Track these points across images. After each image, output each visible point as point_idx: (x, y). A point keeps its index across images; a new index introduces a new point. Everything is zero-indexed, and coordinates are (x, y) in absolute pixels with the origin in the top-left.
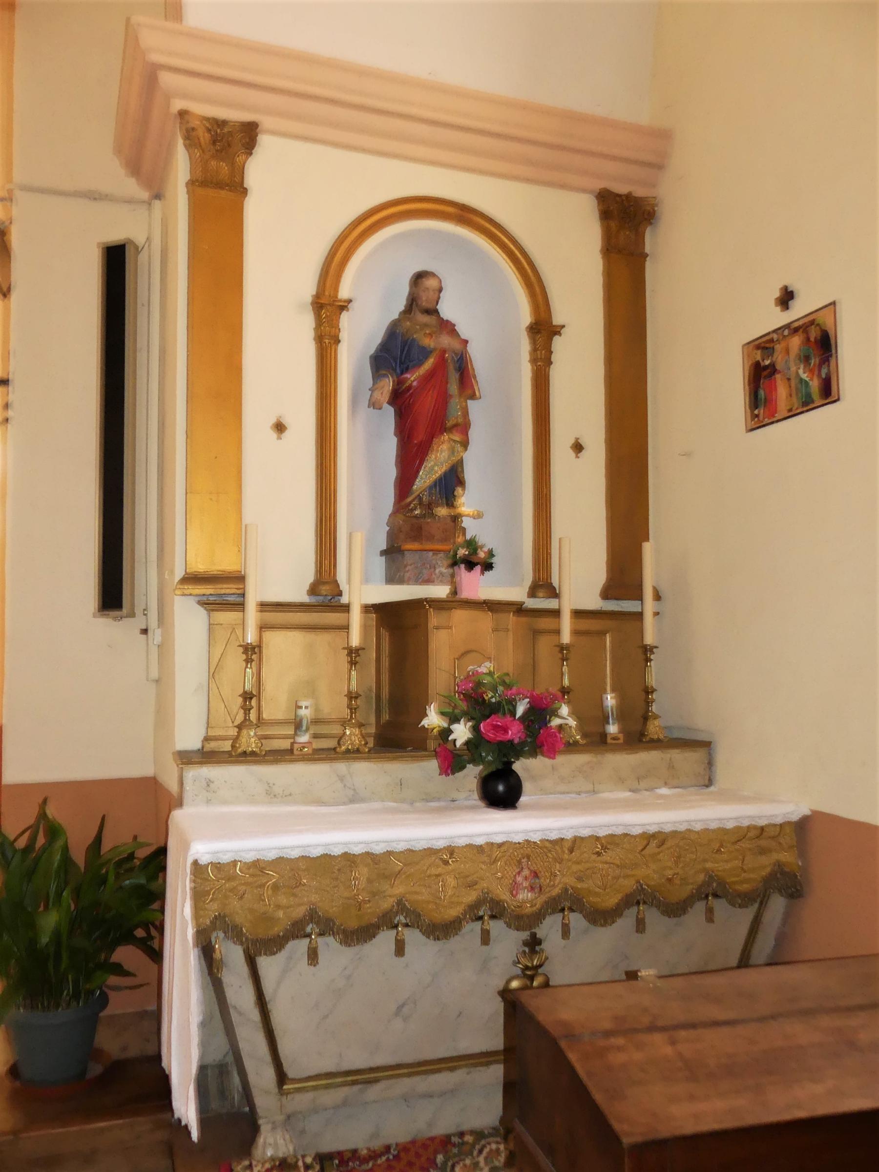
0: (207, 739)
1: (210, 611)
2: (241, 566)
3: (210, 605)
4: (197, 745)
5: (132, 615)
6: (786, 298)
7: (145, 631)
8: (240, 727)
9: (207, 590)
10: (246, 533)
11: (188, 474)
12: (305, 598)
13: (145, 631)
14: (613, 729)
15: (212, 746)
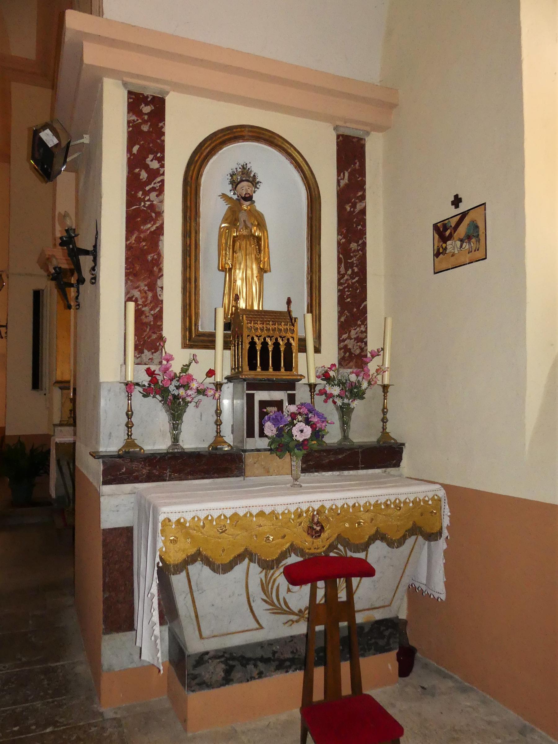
0: (61, 421)
1: (62, 390)
2: (66, 488)
3: (61, 388)
4: (58, 423)
5: (42, 390)
6: (457, 201)
7: (45, 394)
8: (69, 418)
9: (62, 385)
10: (75, 328)
11: (193, 614)
12: (267, 447)
13: (45, 394)
14: (362, 509)
15: (63, 422)
